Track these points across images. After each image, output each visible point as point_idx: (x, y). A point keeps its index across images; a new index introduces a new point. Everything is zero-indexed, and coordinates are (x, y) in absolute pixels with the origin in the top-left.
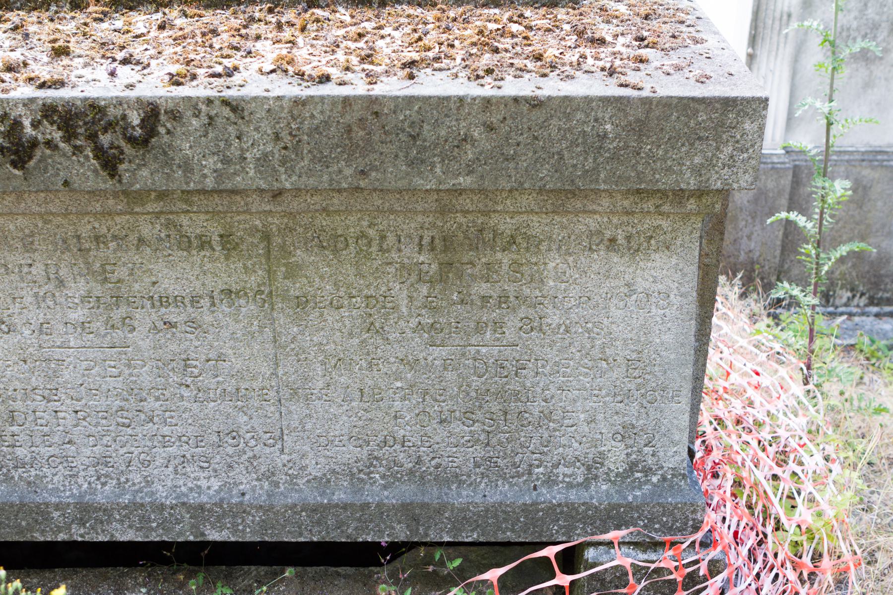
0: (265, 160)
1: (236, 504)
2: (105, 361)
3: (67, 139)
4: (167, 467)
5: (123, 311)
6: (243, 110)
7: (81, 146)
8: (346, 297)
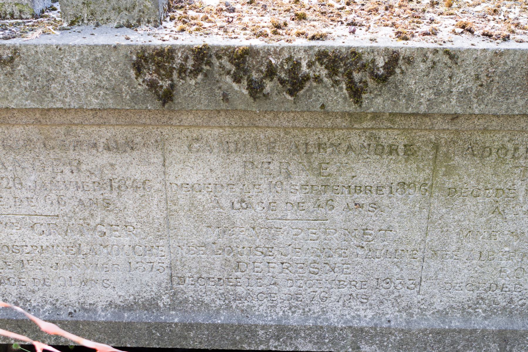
0: (465, 94)
1: (386, 328)
2: (309, 229)
3: (329, 76)
4: (338, 302)
5: (328, 195)
6: (457, 58)
7: (339, 81)
8: (483, 189)
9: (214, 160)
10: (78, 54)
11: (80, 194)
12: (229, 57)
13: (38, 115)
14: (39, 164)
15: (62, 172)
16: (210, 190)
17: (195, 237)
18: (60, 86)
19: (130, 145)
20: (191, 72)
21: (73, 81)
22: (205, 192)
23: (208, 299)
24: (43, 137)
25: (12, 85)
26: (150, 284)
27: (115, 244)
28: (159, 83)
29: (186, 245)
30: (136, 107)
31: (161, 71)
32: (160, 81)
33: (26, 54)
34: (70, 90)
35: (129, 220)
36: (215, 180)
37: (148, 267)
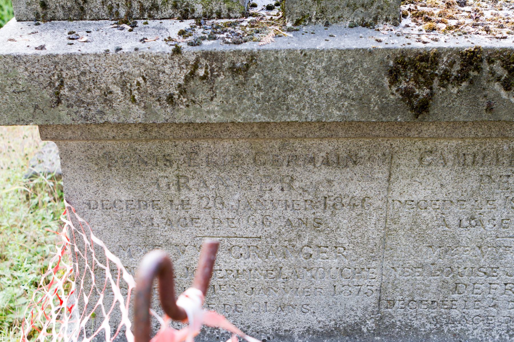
9: (446, 174)
10: (326, 60)
11: (289, 214)
12: (503, 61)
13: (255, 128)
14: (246, 182)
15: (271, 190)
16: (437, 207)
17: (413, 257)
18: (299, 97)
19: (353, 159)
20: (456, 78)
21: (314, 90)
22: (431, 209)
23: (418, 323)
24: (254, 152)
25: (243, 96)
26: (355, 309)
27: (321, 266)
28: (415, 92)
29: (401, 266)
30: (384, 119)
31: (420, 78)
32: (417, 90)
33: (263, 61)
34: (309, 101)
35: (340, 240)
36: (445, 196)
37: (354, 290)
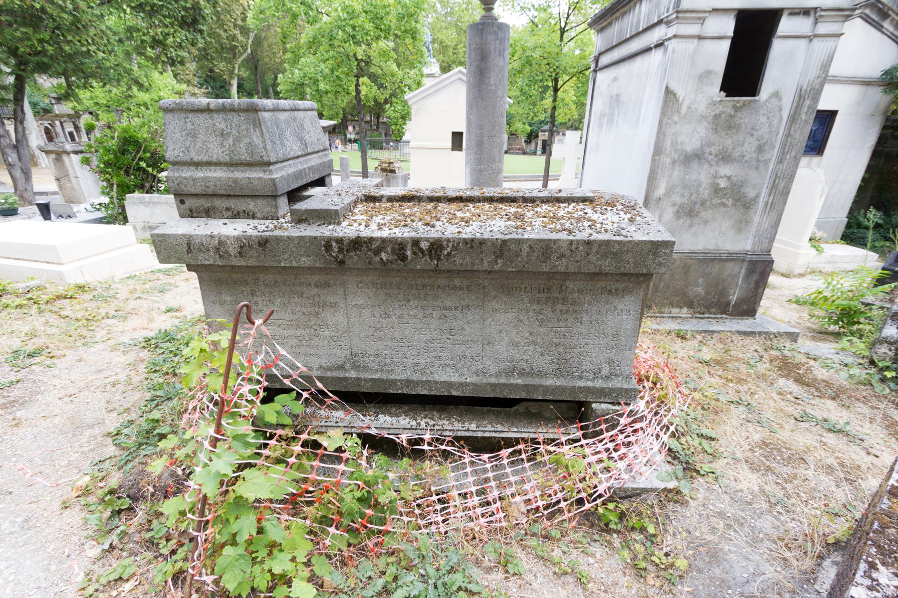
11: (303, 309)
19: (327, 285)
